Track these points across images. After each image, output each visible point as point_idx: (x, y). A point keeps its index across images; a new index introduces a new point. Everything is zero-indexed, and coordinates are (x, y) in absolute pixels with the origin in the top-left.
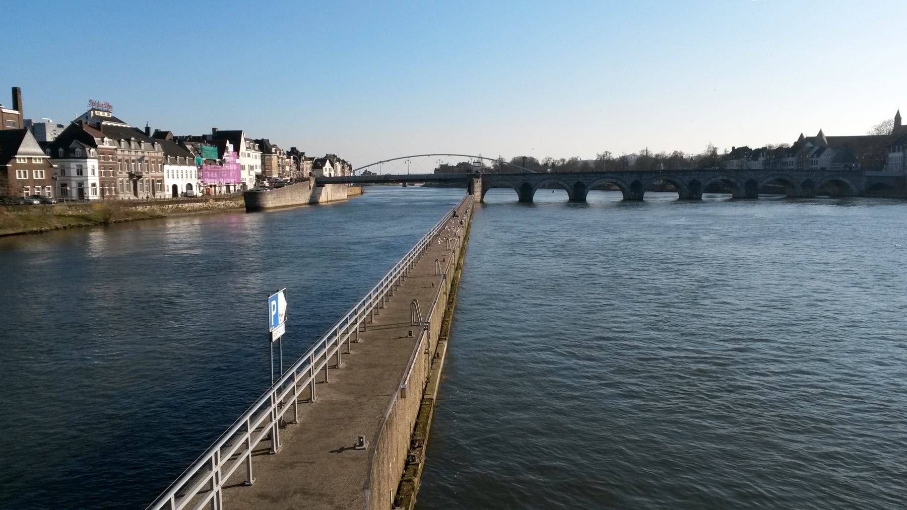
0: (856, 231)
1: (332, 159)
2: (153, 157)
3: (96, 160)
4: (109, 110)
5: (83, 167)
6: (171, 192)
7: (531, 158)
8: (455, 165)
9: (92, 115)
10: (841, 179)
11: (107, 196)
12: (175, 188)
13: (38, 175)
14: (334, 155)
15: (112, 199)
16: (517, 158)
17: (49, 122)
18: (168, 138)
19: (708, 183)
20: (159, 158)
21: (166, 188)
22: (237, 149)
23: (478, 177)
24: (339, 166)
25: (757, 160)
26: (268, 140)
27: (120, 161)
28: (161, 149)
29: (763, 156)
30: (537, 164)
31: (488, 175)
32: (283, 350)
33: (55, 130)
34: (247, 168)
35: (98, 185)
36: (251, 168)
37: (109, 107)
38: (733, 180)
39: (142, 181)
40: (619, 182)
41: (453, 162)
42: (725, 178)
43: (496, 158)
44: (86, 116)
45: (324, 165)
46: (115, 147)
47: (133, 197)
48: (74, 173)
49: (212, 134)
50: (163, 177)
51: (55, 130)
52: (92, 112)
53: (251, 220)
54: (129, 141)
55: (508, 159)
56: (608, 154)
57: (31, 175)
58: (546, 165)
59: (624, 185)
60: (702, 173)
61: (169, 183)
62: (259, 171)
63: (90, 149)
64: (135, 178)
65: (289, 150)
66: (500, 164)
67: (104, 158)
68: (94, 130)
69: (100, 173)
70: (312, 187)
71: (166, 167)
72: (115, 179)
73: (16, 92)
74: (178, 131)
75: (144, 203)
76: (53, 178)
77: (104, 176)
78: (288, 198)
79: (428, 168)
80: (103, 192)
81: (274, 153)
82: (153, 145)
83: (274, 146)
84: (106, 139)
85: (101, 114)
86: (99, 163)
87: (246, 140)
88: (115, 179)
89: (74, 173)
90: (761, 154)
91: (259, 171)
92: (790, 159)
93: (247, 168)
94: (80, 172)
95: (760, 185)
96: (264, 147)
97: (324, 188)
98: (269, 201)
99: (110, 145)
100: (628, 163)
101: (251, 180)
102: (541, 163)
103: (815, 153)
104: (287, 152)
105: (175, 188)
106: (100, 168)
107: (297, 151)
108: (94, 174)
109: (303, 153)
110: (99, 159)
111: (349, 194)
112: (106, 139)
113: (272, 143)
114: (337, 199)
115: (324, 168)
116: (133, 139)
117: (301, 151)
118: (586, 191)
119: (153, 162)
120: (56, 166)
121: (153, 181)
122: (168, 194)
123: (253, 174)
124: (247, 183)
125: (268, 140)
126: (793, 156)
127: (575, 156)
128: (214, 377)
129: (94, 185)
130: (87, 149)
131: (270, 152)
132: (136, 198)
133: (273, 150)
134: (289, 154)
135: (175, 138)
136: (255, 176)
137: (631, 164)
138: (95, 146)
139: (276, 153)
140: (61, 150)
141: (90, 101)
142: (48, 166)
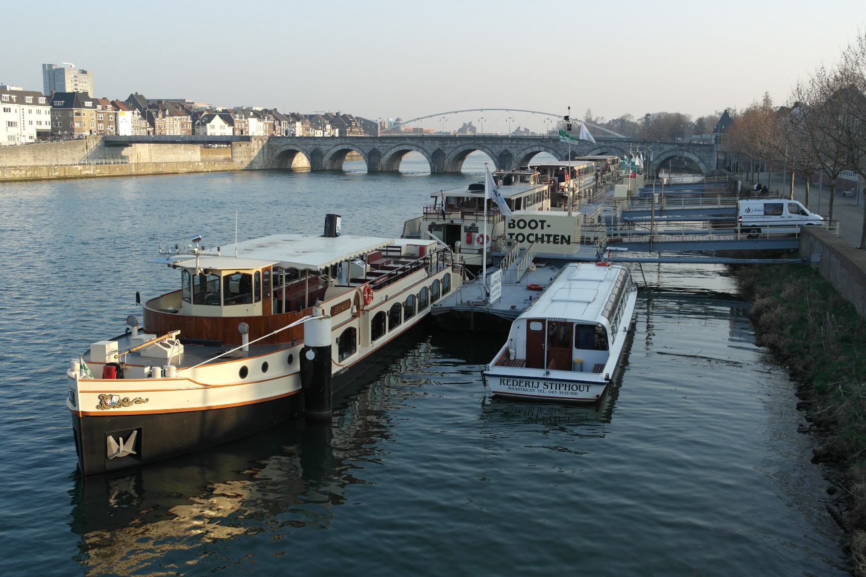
60: (515, 142)
115: (208, 125)
127: (682, 113)
141: (766, 93)
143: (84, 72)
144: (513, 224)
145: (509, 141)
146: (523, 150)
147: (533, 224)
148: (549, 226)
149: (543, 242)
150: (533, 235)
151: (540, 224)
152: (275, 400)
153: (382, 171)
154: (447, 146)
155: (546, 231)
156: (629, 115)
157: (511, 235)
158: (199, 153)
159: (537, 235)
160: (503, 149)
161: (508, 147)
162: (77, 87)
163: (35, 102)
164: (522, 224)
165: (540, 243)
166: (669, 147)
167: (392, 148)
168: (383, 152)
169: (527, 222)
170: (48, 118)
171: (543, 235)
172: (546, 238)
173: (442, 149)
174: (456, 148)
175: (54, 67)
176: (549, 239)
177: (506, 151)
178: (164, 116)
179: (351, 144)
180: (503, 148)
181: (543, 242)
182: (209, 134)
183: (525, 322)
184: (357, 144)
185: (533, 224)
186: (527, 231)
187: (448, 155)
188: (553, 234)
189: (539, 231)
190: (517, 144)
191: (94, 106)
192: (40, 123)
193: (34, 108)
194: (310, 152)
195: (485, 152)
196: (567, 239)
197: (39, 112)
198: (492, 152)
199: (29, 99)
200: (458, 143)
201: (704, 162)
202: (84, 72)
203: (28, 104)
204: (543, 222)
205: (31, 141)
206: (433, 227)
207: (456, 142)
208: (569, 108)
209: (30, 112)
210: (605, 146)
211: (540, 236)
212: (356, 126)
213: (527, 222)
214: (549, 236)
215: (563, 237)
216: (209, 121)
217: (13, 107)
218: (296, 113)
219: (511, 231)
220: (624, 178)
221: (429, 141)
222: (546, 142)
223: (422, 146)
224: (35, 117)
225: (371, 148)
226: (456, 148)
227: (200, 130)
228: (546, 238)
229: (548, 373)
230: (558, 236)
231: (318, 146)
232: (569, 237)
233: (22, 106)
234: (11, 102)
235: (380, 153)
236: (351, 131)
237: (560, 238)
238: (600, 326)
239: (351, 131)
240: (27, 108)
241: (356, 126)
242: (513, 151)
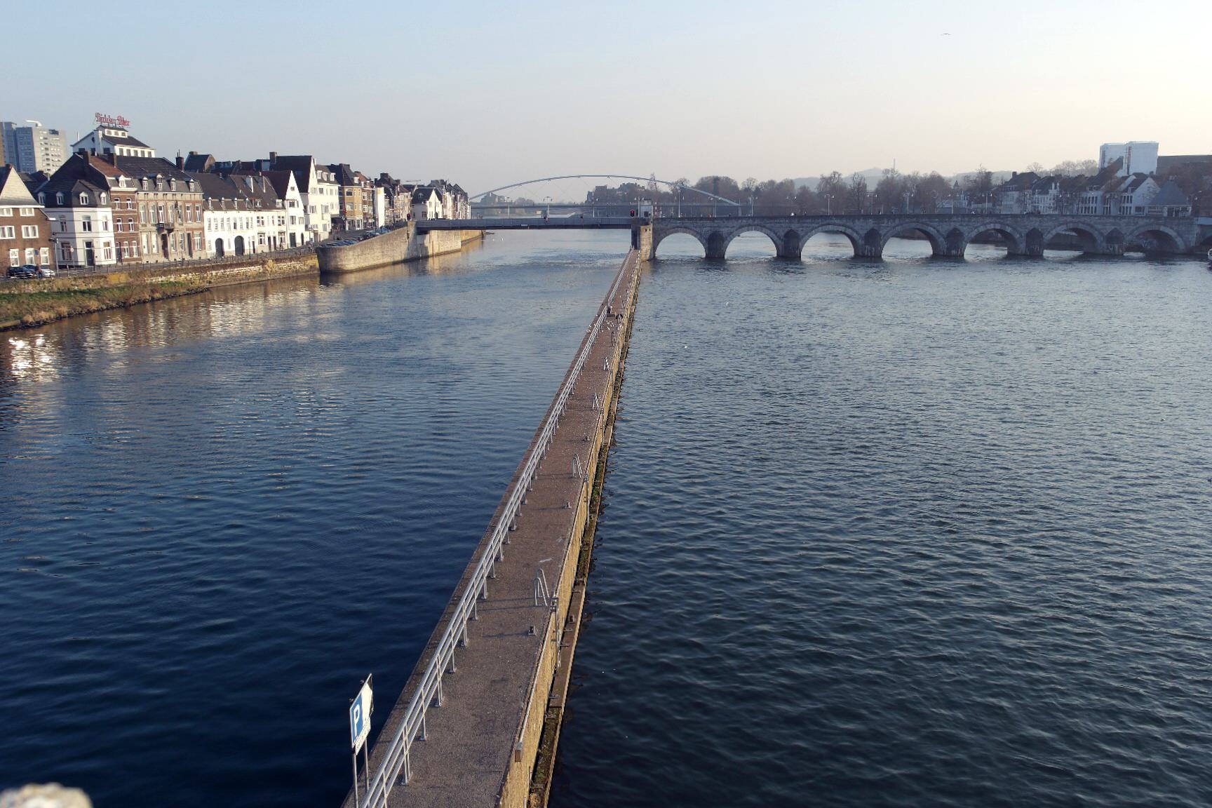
1: (440, 187)
2: (188, 202)
3: (110, 209)
4: (125, 128)
5: (92, 218)
6: (214, 250)
7: (727, 178)
8: (617, 187)
9: (101, 136)
10: (1162, 228)
11: (127, 260)
12: (219, 243)
13: (30, 232)
14: (442, 181)
15: (133, 263)
16: (706, 178)
17: (37, 125)
18: (207, 164)
19: (973, 234)
20: (197, 202)
21: (207, 245)
22: (303, 187)
23: (647, 224)
24: (449, 197)
25: (1047, 193)
26: (349, 165)
28: (199, 188)
29: (1055, 188)
30: (735, 187)
31: (662, 218)
33: (46, 139)
34: (319, 210)
35: (113, 244)
36: (326, 209)
37: (124, 122)
38: (1009, 230)
39: (174, 236)
40: (849, 231)
41: (614, 184)
42: (998, 226)
43: (674, 180)
44: (92, 137)
45: (428, 199)
46: (135, 189)
47: (162, 259)
50: (203, 229)
51: (46, 139)
52: (100, 132)
53: (328, 297)
54: (154, 179)
55: (692, 182)
56: (837, 176)
57: (19, 233)
58: (747, 190)
59: (855, 235)
61: (211, 238)
62: (336, 211)
63: (101, 193)
64: (164, 231)
65: (379, 178)
66: (682, 192)
67: (121, 206)
68: (104, 163)
69: (116, 228)
70: (410, 236)
71: (207, 214)
72: (137, 234)
74: (223, 154)
76: (50, 240)
77: (122, 232)
78: (378, 253)
79: (578, 194)
80: (119, 254)
81: (356, 184)
82: (188, 183)
83: (357, 173)
84: (122, 178)
85: (113, 134)
86: (113, 212)
87: (318, 168)
88: (137, 234)
89: (78, 227)
90: (1053, 185)
91: (336, 211)
92: (1092, 194)
93: (319, 210)
94: (87, 226)
95: (1047, 237)
96: (342, 175)
97: (428, 236)
98: (350, 260)
99: (128, 186)
100: (865, 186)
101: (325, 227)
102: (740, 186)
103: (1129, 186)
104: (376, 179)
105: (219, 243)
106: (115, 220)
107: (390, 179)
108: (106, 228)
109: (398, 181)
110: (113, 207)
111: (464, 239)
112: (122, 178)
113: (353, 169)
114: (446, 250)
116: (159, 176)
117: (394, 178)
118: (800, 244)
119: (188, 208)
120: (54, 219)
121: (189, 235)
122: (211, 251)
123: (328, 218)
124: (320, 230)
125: (349, 165)
126: (1097, 189)
127: (721, 173)
129: (108, 244)
130: (96, 194)
131: (351, 183)
132: (166, 260)
133: (356, 180)
134: (378, 183)
135: (218, 164)
136: (330, 219)
137: (871, 187)
138: (107, 189)
139: (359, 184)
141: (98, 115)
142: (41, 219)
143: (54, 132)
146: (976, 228)
152: (346, 795)
153: (944, 256)
156: (685, 180)
160: (952, 228)
161: (957, 225)
162: (48, 152)
166: (1145, 221)
168: (800, 233)
174: (894, 227)
175: (14, 127)
177: (955, 229)
180: (952, 225)
184: (768, 225)
190: (969, 221)
194: (707, 236)
200: (897, 221)
201: (1181, 237)
202: (54, 132)
207: (894, 219)
210: (1071, 222)
220: (658, 253)
221: (861, 220)
222: (1003, 219)
225: (786, 230)
226: (894, 227)
242: (964, 229)
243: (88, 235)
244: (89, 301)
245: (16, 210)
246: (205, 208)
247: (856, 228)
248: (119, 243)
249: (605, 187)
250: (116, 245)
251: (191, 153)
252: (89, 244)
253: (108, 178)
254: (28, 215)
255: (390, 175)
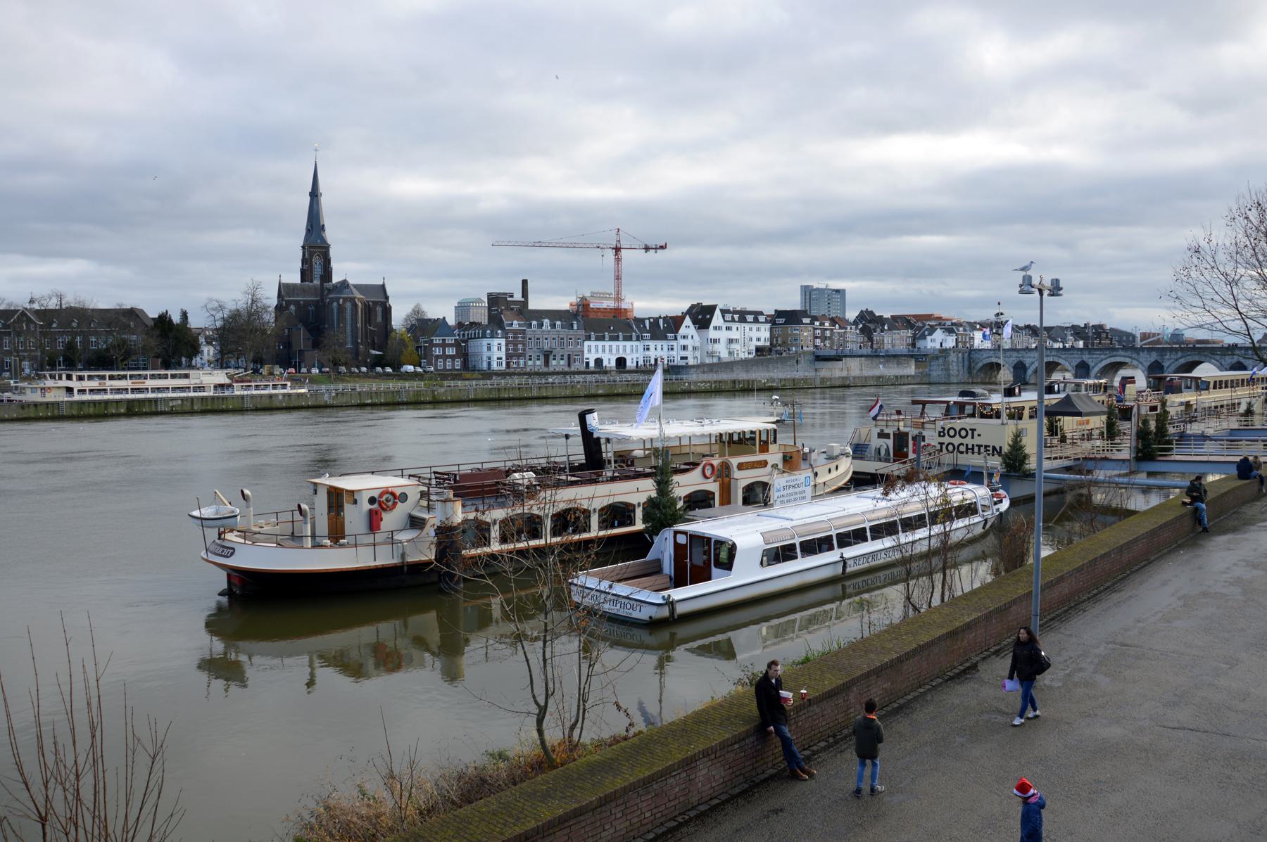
0: (358, 785)
6: (613, 364)
27: (530, 339)
32: (150, 366)
35: (504, 358)
48: (485, 349)
49: (530, 308)
69: (507, 350)
71: (587, 343)
73: (525, 283)
75: (519, 374)
80: (508, 364)
94: (489, 349)
106: (507, 345)
112: (515, 322)
115: (929, 338)
121: (569, 355)
128: (135, 365)
138: (503, 328)
140: (488, 331)
144: (943, 432)
145: (1243, 352)
147: (963, 433)
148: (979, 435)
149: (973, 453)
150: (963, 444)
151: (970, 432)
154: (1167, 357)
155: (977, 441)
157: (941, 444)
158: (913, 367)
159: (967, 445)
163: (756, 321)
164: (952, 432)
165: (970, 454)
167: (1102, 360)
168: (1091, 364)
169: (958, 431)
170: (768, 335)
171: (973, 445)
172: (976, 449)
173: (1160, 361)
174: (1177, 360)
176: (979, 450)
178: (882, 331)
179: (1056, 356)
181: (973, 453)
182: (929, 347)
183: (672, 534)
185: (963, 433)
186: (957, 440)
187: (1168, 367)
188: (984, 444)
189: (969, 441)
191: (812, 323)
192: (758, 339)
193: (754, 326)
195: (1213, 364)
196: (998, 450)
197: (758, 330)
198: (1221, 364)
199: (750, 318)
203: (761, 323)
204: (973, 430)
205: (751, 356)
206: (1170, 442)
207: (1177, 353)
208: (999, 304)
209: (751, 329)
211: (970, 447)
212: (1107, 338)
213: (958, 431)
214: (979, 446)
215: (994, 448)
216: (930, 334)
217: (734, 326)
218: (1032, 324)
219: (942, 439)
223: (1136, 357)
224: (754, 334)
225: (1079, 361)
227: (920, 344)
228: (976, 449)
229: (611, 587)
230: (989, 446)
231: (1021, 359)
232: (1001, 448)
233: (743, 325)
234: (733, 320)
235: (1089, 366)
236: (1100, 343)
237: (991, 449)
238: (730, 543)
239: (1100, 343)
240: (747, 326)
241: (1107, 338)
243: (489, 354)
244: (1072, 335)
245: (444, 340)
246: (588, 338)
247: (1141, 360)
248: (509, 356)
249: (932, 315)
250: (507, 359)
251: (490, 295)
252: (490, 358)
253: (505, 322)
254: (438, 342)
255: (302, 244)
